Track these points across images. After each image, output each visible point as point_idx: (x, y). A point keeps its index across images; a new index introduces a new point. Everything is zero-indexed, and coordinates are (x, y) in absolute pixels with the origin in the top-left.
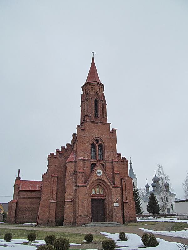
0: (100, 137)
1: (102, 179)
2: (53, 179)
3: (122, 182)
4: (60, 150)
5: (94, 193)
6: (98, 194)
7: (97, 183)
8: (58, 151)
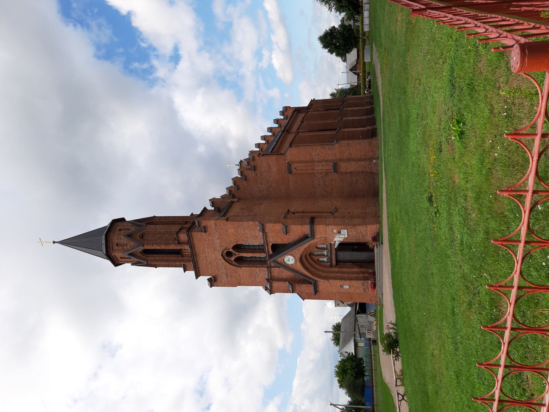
6: (325, 253)
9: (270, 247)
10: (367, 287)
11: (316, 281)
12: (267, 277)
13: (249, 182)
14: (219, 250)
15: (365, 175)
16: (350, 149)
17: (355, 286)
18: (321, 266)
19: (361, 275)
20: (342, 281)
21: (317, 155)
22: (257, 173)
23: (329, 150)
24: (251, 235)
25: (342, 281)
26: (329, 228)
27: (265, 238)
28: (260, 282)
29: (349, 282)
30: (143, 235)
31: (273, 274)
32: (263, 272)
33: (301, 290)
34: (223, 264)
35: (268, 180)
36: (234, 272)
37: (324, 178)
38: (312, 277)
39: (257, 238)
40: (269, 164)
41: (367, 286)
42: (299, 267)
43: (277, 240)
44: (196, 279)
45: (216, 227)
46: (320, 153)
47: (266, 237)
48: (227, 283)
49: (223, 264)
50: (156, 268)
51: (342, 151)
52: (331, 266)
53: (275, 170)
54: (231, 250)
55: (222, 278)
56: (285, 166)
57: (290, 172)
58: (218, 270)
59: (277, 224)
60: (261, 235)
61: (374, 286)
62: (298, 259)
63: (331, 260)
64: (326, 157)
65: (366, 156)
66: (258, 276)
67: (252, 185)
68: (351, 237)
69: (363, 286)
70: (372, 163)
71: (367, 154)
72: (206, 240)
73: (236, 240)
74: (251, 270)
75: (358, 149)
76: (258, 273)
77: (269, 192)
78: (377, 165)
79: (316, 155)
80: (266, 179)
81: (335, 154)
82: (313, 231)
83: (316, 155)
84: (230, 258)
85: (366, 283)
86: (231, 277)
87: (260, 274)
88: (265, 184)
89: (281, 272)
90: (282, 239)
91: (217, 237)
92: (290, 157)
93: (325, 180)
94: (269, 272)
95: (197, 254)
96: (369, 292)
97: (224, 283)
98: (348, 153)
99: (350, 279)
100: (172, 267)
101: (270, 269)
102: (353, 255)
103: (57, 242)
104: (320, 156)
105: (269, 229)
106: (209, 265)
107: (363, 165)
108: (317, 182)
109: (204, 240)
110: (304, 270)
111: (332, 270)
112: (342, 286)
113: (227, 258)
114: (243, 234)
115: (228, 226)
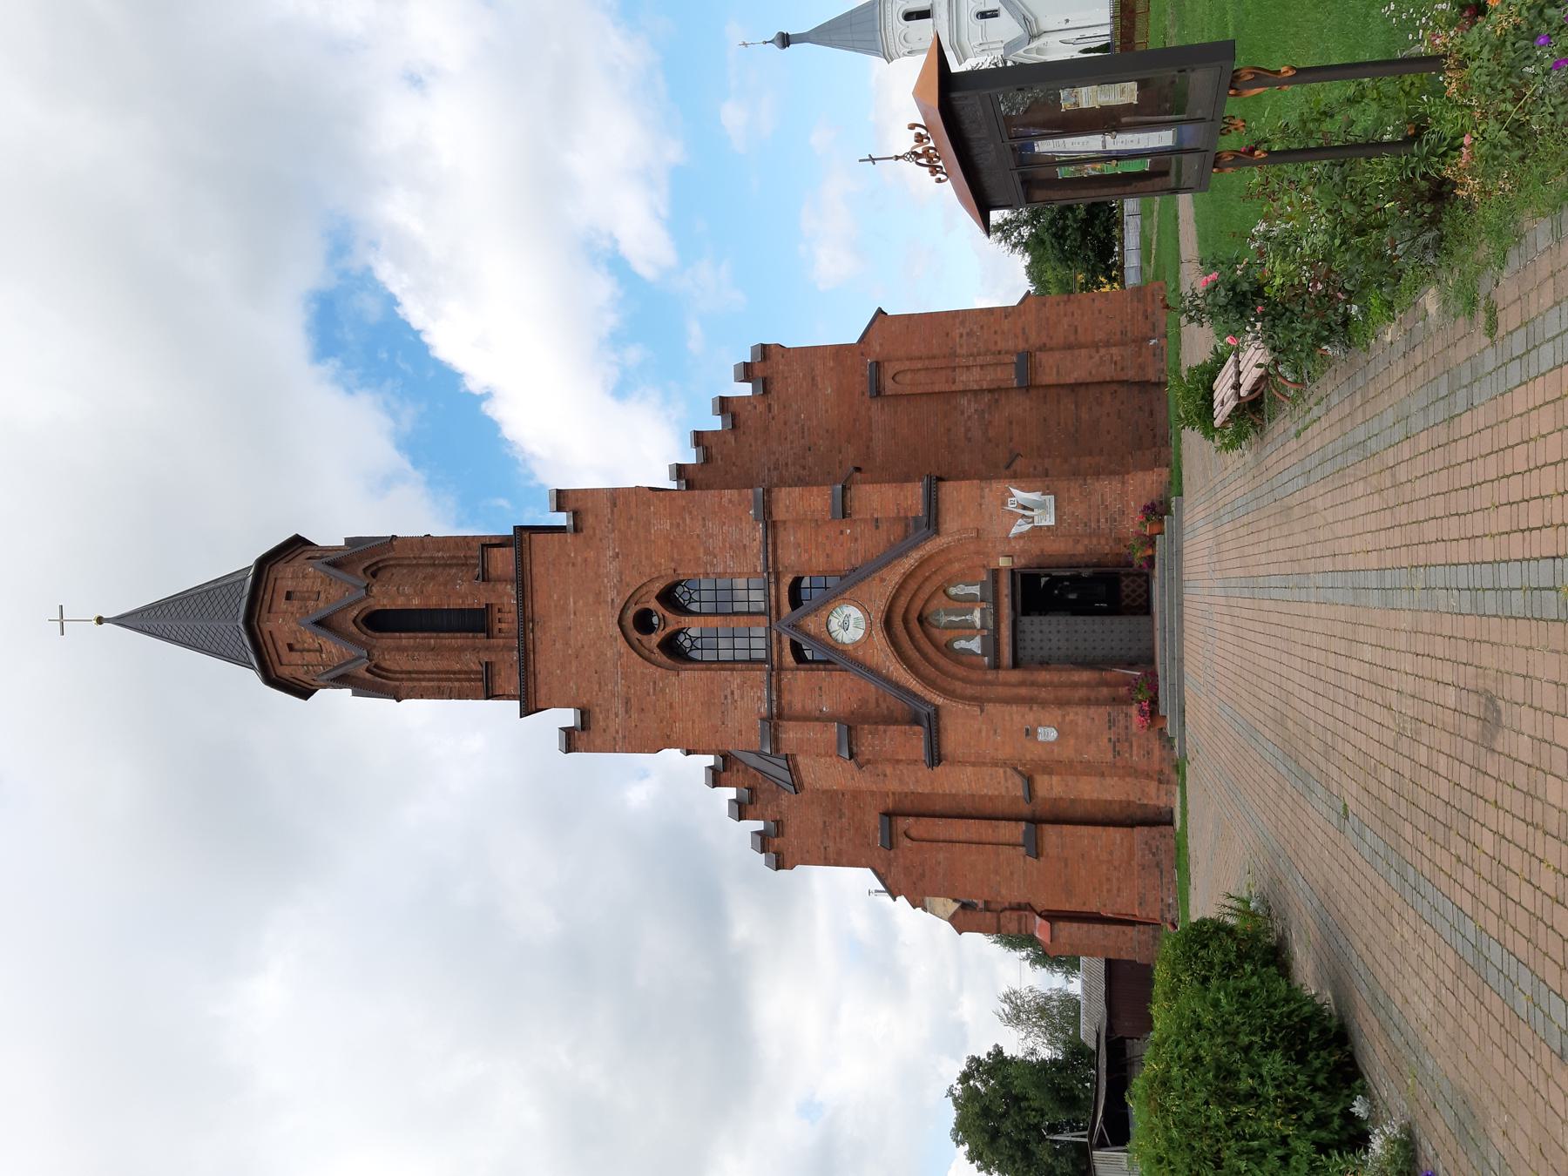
0: (619, 603)
1: (882, 604)
2: (907, 843)
3: (896, 396)
4: (730, 793)
5: (975, 645)
6: (976, 617)
7: (915, 625)
8: (741, 810)
9: (787, 589)
10: (1127, 734)
11: (937, 709)
12: (764, 709)
13: (744, 433)
14: (613, 600)
15: (1122, 403)
16: (1073, 314)
17: (1080, 730)
18: (961, 663)
19: (1105, 691)
20: (1031, 709)
21: (968, 334)
22: (773, 403)
23: (1006, 317)
24: (724, 541)
25: (1031, 709)
26: (991, 491)
27: (770, 550)
28: (740, 731)
29: (1060, 712)
30: (379, 569)
31: (786, 697)
32: (752, 688)
33: (881, 750)
34: (621, 655)
35: (803, 425)
36: (654, 689)
37: (986, 416)
38: (926, 692)
39: (745, 554)
40: (813, 370)
41: (1127, 728)
42: (882, 656)
43: (810, 558)
44: (521, 717)
45: (612, 511)
46: (975, 328)
47: (775, 544)
48: (624, 737)
49: (621, 655)
50: (399, 701)
51: (1048, 319)
52: (996, 666)
53: (829, 391)
54: (654, 605)
55: (608, 717)
56: (863, 375)
57: (878, 392)
58: (600, 684)
59: (815, 488)
60: (758, 540)
61: (1152, 711)
62: (878, 618)
63: (997, 642)
64: (996, 343)
65: (1126, 335)
66: (736, 708)
67: (751, 446)
68: (1069, 524)
69: (1110, 728)
70: (1144, 350)
71: (1129, 329)
72: (573, 565)
73: (673, 560)
74: (712, 683)
75: (1100, 312)
76: (735, 693)
77: (804, 468)
78: (1162, 355)
79: (964, 335)
80: (797, 423)
81: (1024, 329)
82: (937, 503)
83: (964, 335)
84: (644, 638)
85: (1122, 717)
86: (643, 710)
87: (742, 698)
88: (792, 442)
89: (817, 689)
90: (828, 556)
91: (614, 549)
92: (881, 345)
93: (990, 422)
94: (774, 685)
95: (536, 620)
96: (1131, 756)
97: (615, 738)
98: (1066, 327)
99: (1062, 703)
100: (451, 699)
101: (778, 674)
102: (1076, 632)
103: (108, 620)
104: (974, 340)
105: (788, 507)
106: (570, 663)
107: (1115, 358)
108: (963, 429)
109: (567, 564)
110: (898, 665)
111: (997, 678)
112: (1030, 733)
113: (635, 635)
114: (698, 536)
115: (652, 508)
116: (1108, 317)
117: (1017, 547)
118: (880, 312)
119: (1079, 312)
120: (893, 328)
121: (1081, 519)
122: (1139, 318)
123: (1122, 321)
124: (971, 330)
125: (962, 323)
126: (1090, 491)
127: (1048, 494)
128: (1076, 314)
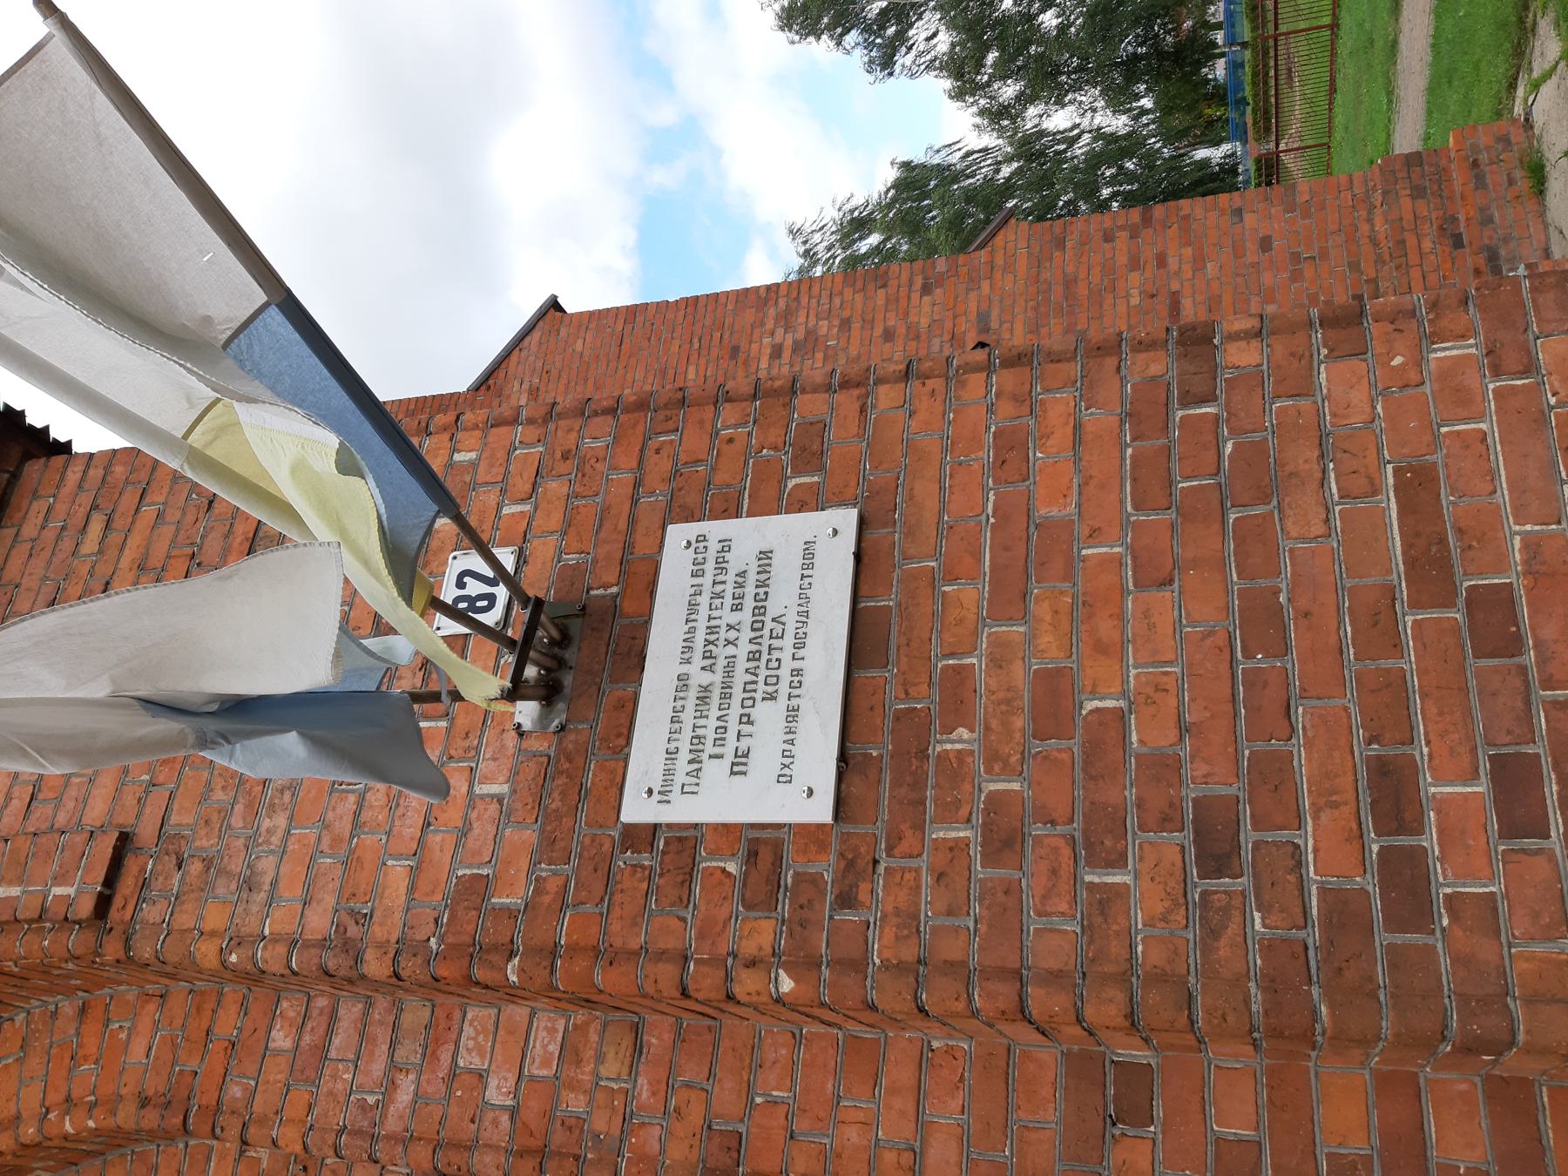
16: (1161, 261)
21: (797, 348)
51: (1070, 283)
75: (1266, 244)
98: (1135, 301)
116: (1296, 258)
117: (498, 1092)
118: (554, 305)
119: (1188, 251)
120: (579, 346)
121: (1162, 768)
122: (1427, 245)
123: (1354, 266)
124: (808, 333)
125: (786, 318)
126: (1252, 455)
127: (803, 503)
128: (1173, 262)
